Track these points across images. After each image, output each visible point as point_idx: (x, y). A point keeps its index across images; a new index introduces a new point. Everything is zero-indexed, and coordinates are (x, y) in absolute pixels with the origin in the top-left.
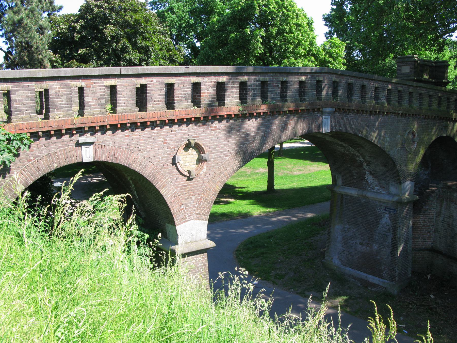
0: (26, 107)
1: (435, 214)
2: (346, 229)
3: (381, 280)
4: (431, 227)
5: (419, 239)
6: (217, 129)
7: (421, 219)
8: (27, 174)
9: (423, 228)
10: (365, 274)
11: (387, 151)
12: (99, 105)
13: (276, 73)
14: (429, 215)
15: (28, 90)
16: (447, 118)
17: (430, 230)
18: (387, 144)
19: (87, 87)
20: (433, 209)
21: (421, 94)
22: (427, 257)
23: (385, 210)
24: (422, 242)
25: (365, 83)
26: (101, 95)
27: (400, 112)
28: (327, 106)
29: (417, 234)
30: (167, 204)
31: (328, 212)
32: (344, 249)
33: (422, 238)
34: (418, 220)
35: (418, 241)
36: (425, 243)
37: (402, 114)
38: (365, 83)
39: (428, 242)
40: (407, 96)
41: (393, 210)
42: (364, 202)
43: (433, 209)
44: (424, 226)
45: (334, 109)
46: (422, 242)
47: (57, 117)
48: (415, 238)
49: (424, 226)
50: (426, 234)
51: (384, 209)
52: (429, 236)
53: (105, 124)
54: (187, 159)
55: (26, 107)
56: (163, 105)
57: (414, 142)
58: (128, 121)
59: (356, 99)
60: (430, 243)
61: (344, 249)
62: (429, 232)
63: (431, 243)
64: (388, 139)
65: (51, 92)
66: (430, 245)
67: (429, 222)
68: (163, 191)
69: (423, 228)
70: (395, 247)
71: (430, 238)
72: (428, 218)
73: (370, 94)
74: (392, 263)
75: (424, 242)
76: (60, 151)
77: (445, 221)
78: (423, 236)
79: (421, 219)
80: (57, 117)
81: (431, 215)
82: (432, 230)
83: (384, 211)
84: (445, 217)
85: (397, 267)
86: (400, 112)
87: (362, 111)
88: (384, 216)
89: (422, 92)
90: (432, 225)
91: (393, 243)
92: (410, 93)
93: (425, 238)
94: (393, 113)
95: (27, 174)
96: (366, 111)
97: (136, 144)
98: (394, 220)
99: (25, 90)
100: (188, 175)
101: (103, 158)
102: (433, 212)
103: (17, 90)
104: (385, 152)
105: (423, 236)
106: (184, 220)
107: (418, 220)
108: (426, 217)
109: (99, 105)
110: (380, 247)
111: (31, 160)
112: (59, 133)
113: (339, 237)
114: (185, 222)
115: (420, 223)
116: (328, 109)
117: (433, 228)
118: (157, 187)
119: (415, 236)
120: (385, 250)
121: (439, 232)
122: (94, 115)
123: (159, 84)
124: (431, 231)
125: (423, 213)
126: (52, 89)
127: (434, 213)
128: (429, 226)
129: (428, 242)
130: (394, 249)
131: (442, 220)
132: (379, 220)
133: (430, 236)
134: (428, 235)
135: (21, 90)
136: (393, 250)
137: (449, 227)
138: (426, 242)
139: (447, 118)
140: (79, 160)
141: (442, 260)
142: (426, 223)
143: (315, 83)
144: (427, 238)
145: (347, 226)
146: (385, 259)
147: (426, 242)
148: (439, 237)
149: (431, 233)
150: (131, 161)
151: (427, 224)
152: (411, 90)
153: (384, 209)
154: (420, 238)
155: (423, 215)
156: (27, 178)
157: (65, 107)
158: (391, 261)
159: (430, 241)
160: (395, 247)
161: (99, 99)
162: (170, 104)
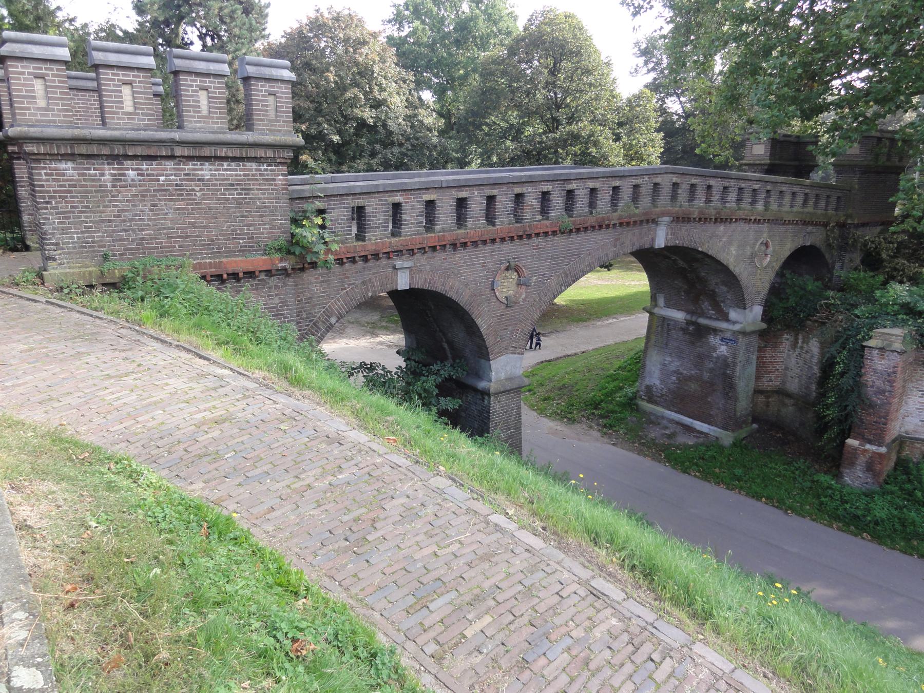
0: (342, 228)
2: (666, 362)
3: (712, 428)
6: (540, 248)
8: (341, 304)
10: (691, 420)
11: (731, 267)
12: (417, 223)
13: (607, 177)
15: (344, 208)
16: (813, 222)
18: (731, 260)
19: (406, 202)
21: (781, 192)
23: (722, 340)
25: (712, 182)
26: (420, 212)
27: (753, 218)
28: (663, 214)
30: (482, 336)
31: (642, 345)
37: (755, 220)
38: (712, 182)
40: (763, 195)
45: (672, 219)
47: (373, 238)
53: (424, 246)
54: (505, 284)
55: (342, 228)
56: (482, 221)
57: (766, 255)
58: (448, 242)
59: (700, 202)
64: (734, 252)
65: (368, 209)
68: (479, 322)
73: (716, 197)
76: (376, 277)
80: (373, 238)
83: (720, 342)
86: (753, 218)
87: (706, 219)
89: (784, 189)
92: (768, 191)
94: (743, 219)
95: (341, 304)
96: (711, 219)
97: (453, 268)
99: (341, 208)
100: (506, 302)
101: (419, 285)
103: (334, 209)
104: (729, 269)
106: (500, 353)
109: (417, 223)
111: (345, 289)
112: (376, 256)
114: (500, 356)
116: (666, 219)
118: (473, 316)
122: (411, 235)
123: (481, 196)
126: (369, 205)
135: (338, 208)
139: (813, 222)
140: (395, 288)
143: (651, 186)
145: (668, 359)
150: (447, 288)
152: (769, 188)
156: (341, 309)
157: (382, 227)
161: (417, 216)
162: (490, 217)
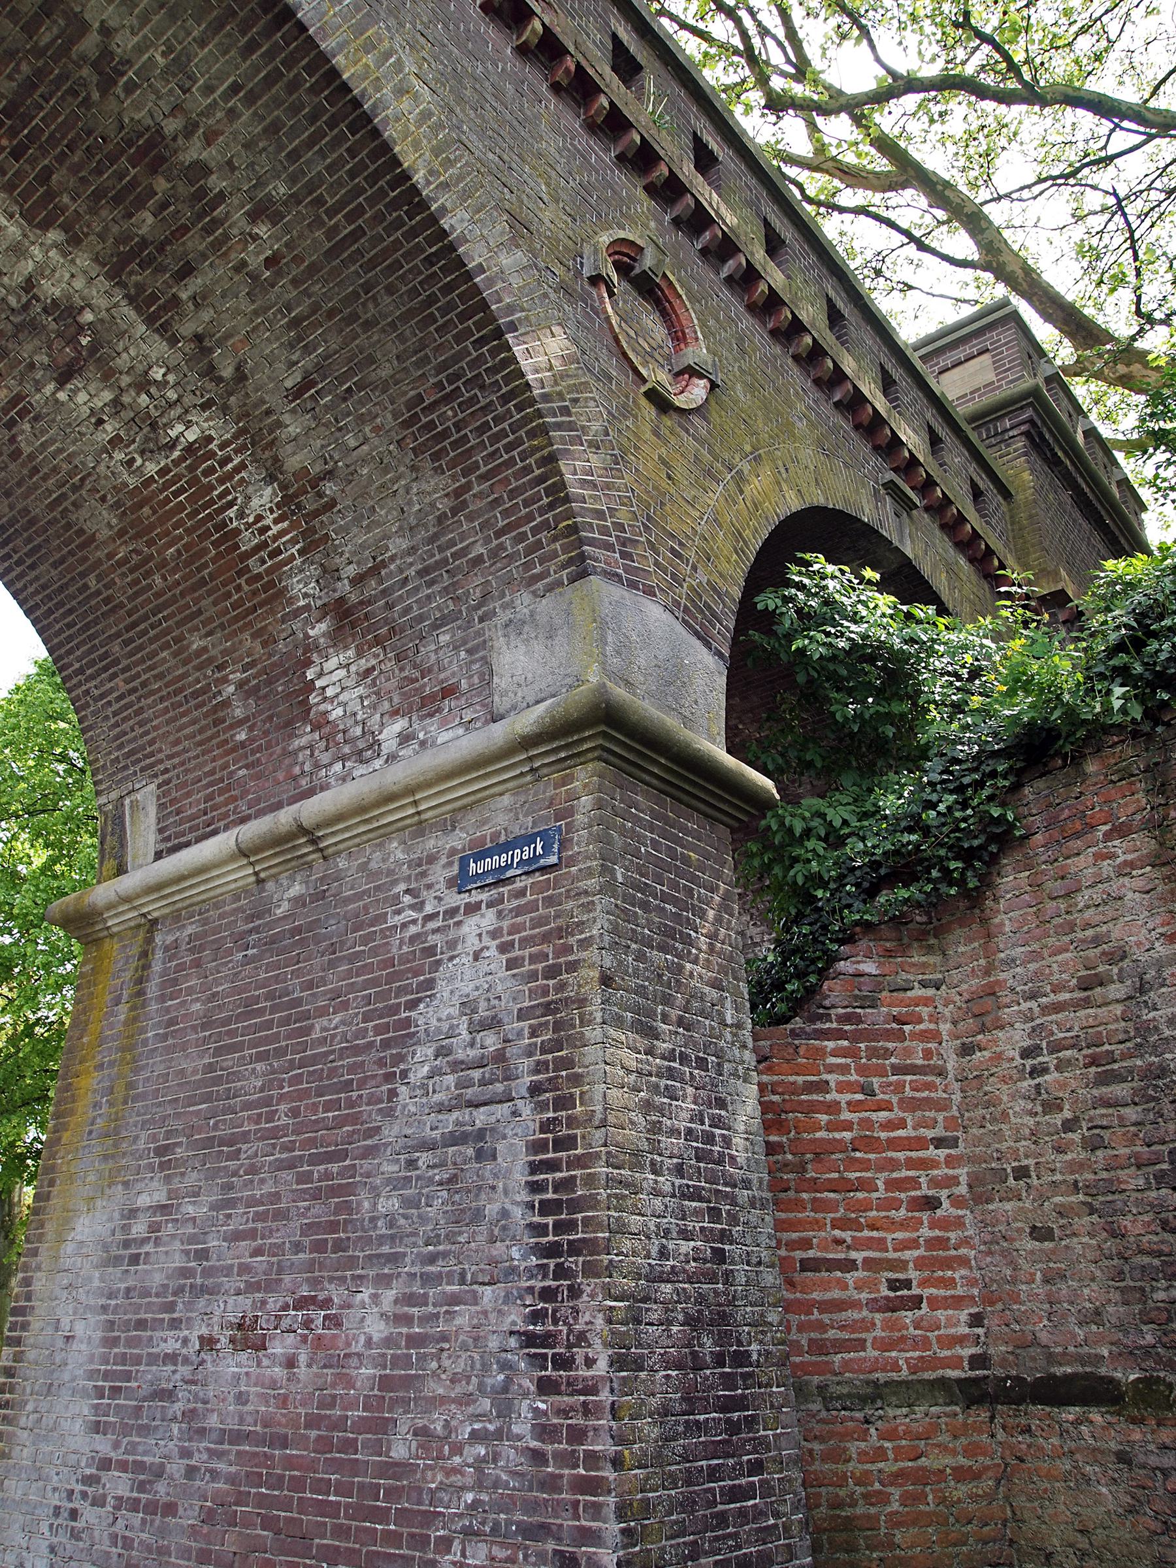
1: (945, 1028)
4: (932, 1152)
5: (850, 1277)
7: (832, 1078)
9: (865, 1165)
14: (900, 1036)
17: (935, 1183)
20: (918, 992)
22: (961, 1474)
24: (876, 1305)
29: (818, 1225)
32: (103, 1445)
33: (868, 1263)
34: (810, 1087)
35: (836, 1294)
36: (908, 1316)
39: (934, 1303)
41: (529, 840)
42: (298, 901)
43: (918, 992)
44: (870, 1143)
46: (876, 1305)
48: (806, 1265)
49: (870, 1143)
50: (903, 1225)
51: (451, 883)
52: (932, 1243)
60: (958, 1321)
61: (103, 1445)
62: (931, 1204)
63: (964, 1316)
66: (961, 1340)
67: (911, 1105)
69: (865, 1165)
70: (575, 1249)
71: (947, 1263)
72: (897, 1070)
74: (551, 1484)
75: (891, 1306)
77: (1055, 1048)
78: (881, 1244)
79: (832, 1078)
81: (914, 1036)
82: (954, 1181)
83: (456, 899)
84: (1046, 1010)
85: (612, 1528)
88: (452, 944)
90: (939, 1132)
91: (546, 1208)
93: (902, 1265)
98: (546, 938)
102: (925, 1011)
105: (881, 1244)
107: (810, 1087)
108: (873, 1053)
110: (422, 1301)
113: (80, 1329)
115: (832, 1108)
117: (950, 1162)
119: (806, 1244)
120: (464, 1317)
121: (1021, 1173)
124: (944, 1194)
125: (843, 1019)
127: (935, 1018)
128: (920, 1143)
129: (934, 1303)
130: (561, 1272)
131: (1026, 1053)
132: (412, 1005)
133: (942, 1243)
134: (926, 1232)
136: (547, 1294)
137: (1104, 1079)
138: (917, 1302)
141: (1123, 1458)
142: (883, 1115)
144: (920, 1264)
146: (475, 1436)
147: (917, 1302)
148: (1040, 1233)
149: (946, 1209)
151: (889, 1125)
153: (451, 883)
154: (850, 1265)
155: (839, 1035)
158: (538, 1457)
159: (957, 1302)
160: (575, 1249)
